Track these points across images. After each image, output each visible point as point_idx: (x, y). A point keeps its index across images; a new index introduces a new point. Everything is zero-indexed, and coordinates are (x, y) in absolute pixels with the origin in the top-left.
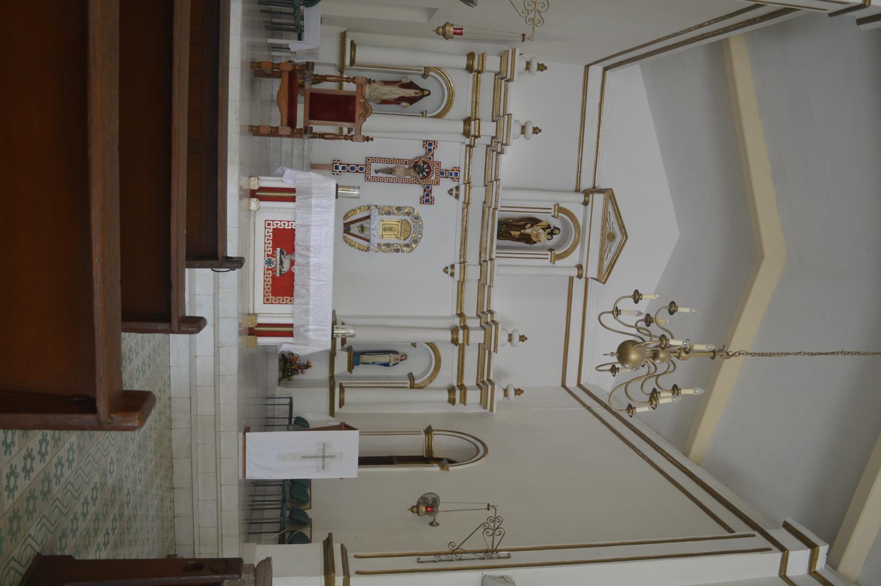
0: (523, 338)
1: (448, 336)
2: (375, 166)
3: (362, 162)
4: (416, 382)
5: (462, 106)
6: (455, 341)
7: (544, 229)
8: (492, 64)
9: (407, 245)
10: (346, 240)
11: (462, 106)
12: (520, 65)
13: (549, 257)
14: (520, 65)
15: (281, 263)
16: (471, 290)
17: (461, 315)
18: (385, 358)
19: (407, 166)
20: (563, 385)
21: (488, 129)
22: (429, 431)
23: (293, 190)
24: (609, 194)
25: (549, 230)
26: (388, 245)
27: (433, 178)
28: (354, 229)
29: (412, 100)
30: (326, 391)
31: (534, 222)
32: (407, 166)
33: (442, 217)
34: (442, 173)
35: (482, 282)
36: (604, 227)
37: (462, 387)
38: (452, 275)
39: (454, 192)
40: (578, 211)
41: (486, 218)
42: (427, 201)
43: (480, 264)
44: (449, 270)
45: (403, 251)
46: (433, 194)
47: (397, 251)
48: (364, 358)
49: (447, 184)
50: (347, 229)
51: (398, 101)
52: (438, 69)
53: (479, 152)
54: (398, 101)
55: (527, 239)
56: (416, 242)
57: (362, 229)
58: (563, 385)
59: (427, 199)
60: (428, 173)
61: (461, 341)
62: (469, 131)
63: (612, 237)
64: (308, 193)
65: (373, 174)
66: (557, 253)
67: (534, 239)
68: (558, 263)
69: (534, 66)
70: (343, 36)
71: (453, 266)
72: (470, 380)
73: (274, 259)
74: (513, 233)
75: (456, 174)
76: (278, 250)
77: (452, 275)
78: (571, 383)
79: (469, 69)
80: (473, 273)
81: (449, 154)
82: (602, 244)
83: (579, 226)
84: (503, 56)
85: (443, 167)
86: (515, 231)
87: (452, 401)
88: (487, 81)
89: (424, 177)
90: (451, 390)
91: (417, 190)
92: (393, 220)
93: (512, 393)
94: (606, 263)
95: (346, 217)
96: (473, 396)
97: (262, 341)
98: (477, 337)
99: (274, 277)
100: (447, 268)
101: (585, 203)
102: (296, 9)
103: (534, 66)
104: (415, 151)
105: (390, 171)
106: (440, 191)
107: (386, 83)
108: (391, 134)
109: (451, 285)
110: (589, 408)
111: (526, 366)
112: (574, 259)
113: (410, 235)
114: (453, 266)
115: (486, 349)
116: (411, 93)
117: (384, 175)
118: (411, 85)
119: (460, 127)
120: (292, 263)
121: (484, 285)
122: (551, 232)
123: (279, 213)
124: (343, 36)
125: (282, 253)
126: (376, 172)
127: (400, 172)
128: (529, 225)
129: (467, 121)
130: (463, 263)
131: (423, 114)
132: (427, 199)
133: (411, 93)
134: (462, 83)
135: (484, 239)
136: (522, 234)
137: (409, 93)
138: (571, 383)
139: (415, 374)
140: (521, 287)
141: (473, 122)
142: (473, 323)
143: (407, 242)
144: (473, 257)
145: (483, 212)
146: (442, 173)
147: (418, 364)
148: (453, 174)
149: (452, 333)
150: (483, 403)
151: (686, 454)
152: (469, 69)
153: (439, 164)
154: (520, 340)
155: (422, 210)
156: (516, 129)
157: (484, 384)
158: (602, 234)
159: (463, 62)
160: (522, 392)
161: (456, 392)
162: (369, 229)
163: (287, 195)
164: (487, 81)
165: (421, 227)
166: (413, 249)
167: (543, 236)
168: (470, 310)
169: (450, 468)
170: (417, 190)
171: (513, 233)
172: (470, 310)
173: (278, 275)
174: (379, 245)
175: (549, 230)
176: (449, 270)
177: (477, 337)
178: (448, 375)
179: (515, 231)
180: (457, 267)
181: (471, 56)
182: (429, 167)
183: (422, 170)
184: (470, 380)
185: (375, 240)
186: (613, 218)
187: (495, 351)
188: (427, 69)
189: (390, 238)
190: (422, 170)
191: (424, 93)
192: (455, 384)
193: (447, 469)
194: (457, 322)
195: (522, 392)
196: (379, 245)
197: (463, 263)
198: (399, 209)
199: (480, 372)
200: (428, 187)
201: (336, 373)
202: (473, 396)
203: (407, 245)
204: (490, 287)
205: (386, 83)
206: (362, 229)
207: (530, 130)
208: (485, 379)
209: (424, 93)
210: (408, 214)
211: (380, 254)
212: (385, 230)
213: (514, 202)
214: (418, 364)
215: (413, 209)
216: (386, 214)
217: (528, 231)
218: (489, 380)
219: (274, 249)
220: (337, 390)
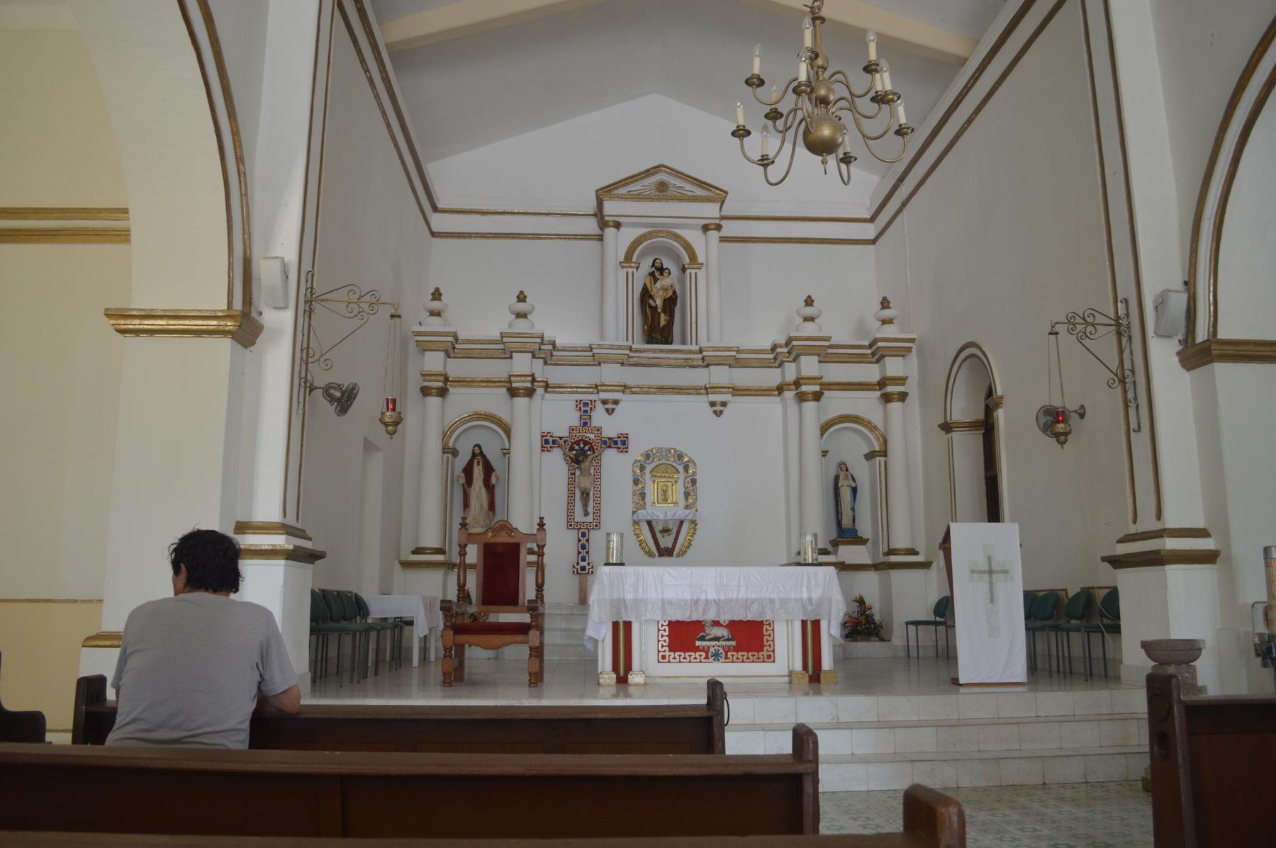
0: (809, 302)
1: (810, 406)
2: (579, 516)
3: (573, 535)
4: (877, 448)
5: (493, 401)
6: (817, 396)
7: (656, 280)
8: (434, 362)
9: (686, 468)
10: (682, 553)
11: (493, 401)
12: (434, 324)
13: (693, 271)
14: (434, 324)
15: (717, 639)
16: (745, 377)
17: (780, 389)
18: (846, 494)
19: (578, 473)
20: (874, 242)
21: (522, 364)
22: (947, 427)
23: (615, 625)
24: (604, 194)
25: (657, 274)
26: (687, 495)
27: (592, 436)
28: (666, 542)
29: (488, 469)
30: (895, 575)
31: (646, 294)
32: (578, 473)
33: (645, 421)
34: (585, 424)
35: (733, 363)
36: (649, 199)
37: (882, 383)
38: (724, 404)
39: (611, 407)
40: (628, 235)
41: (643, 361)
42: (624, 443)
43: (708, 366)
44: (718, 409)
45: (694, 473)
46: (614, 435)
47: (694, 482)
48: (846, 522)
49: (599, 417)
50: (666, 552)
51: (490, 488)
52: (445, 435)
53: (555, 374)
54: (490, 488)
55: (670, 303)
56: (680, 457)
57: (666, 531)
58: (874, 242)
59: (620, 443)
60: (586, 443)
61: (817, 388)
62: (525, 389)
63: (662, 186)
64: (619, 604)
65: (590, 519)
66: (687, 260)
67: (670, 293)
68: (701, 259)
69: (436, 305)
70: (406, 565)
71: (713, 404)
72: (871, 373)
73: (712, 649)
74: (663, 323)
75: (586, 404)
76: (698, 643)
77: (724, 404)
78: (869, 231)
79: (442, 392)
80: (720, 375)
81: (558, 415)
82: (673, 199)
83: (650, 233)
84: (423, 348)
85: (574, 419)
86: (660, 320)
87: (903, 397)
88: (457, 368)
89: (592, 449)
90: (887, 398)
91: (610, 457)
92: (652, 490)
93: (887, 313)
94: (699, 192)
95: (650, 554)
96: (894, 367)
97: (827, 663)
98: (810, 366)
99: (737, 649)
100: (715, 412)
101: (617, 225)
102: (371, 628)
103: (436, 305)
104: (556, 462)
105: (585, 495)
106: (608, 425)
107: (466, 505)
108: (534, 495)
109: (738, 406)
110: (904, 204)
111: (848, 297)
112: (694, 237)
113: (672, 464)
114: (713, 404)
115: (827, 352)
116: (478, 471)
117: (591, 503)
118: (468, 471)
119: (521, 402)
120: (716, 623)
121: (736, 360)
122: (659, 270)
123: (648, 644)
124: (406, 565)
125: (702, 639)
126: (586, 514)
127: (585, 482)
128: (651, 302)
129: (513, 393)
130: (707, 390)
131: (506, 453)
132: (620, 443)
133: (478, 471)
134: (463, 402)
135: (673, 362)
136: (664, 311)
137: (479, 473)
138: (869, 231)
139: (867, 451)
140: (738, 307)
141: (514, 385)
142: (790, 372)
143: (681, 469)
144: (699, 377)
145: (635, 365)
146: (585, 424)
147: (852, 447)
148: (585, 409)
149: (805, 400)
150: (903, 353)
151: (963, 61)
152: (442, 392)
153: (572, 429)
154: (811, 305)
155: (637, 448)
156: (521, 326)
157: (876, 353)
158: (659, 200)
159: (434, 401)
160: (885, 299)
161: (888, 390)
162: (666, 521)
163: (622, 633)
164: (457, 368)
165: (660, 450)
166: (691, 460)
167: (664, 282)
168: (771, 377)
169: (999, 393)
170: (610, 457)
171: (663, 323)
172: (771, 377)
173: (733, 643)
174: (687, 507)
175: (657, 274)
176: (718, 409)
177: (810, 366)
178: (866, 406)
179: (660, 320)
180: (712, 398)
181: (425, 391)
182: (577, 443)
183: (581, 451)
184: (871, 373)
185: (681, 513)
186: (636, 187)
187: (828, 339)
188: (446, 450)
189: (677, 492)
190: (581, 451)
191: (478, 454)
192: (878, 394)
193: (1001, 397)
194: (789, 395)
195: (885, 299)
196: (687, 507)
197: (707, 390)
198: (636, 482)
199: (860, 359)
200: (605, 442)
201: (869, 562)
202: (894, 367)
203: (686, 468)
204: (738, 352)
205: (466, 505)
206: (666, 531)
207: (521, 307)
208: (869, 351)
209: (478, 454)
210: (642, 468)
211: (699, 504)
212: (665, 500)
213: (619, 323)
214: (852, 447)
215: (636, 461)
216: (643, 499)
217: (659, 302)
218: (870, 346)
219: (697, 649)
220: (893, 559)
